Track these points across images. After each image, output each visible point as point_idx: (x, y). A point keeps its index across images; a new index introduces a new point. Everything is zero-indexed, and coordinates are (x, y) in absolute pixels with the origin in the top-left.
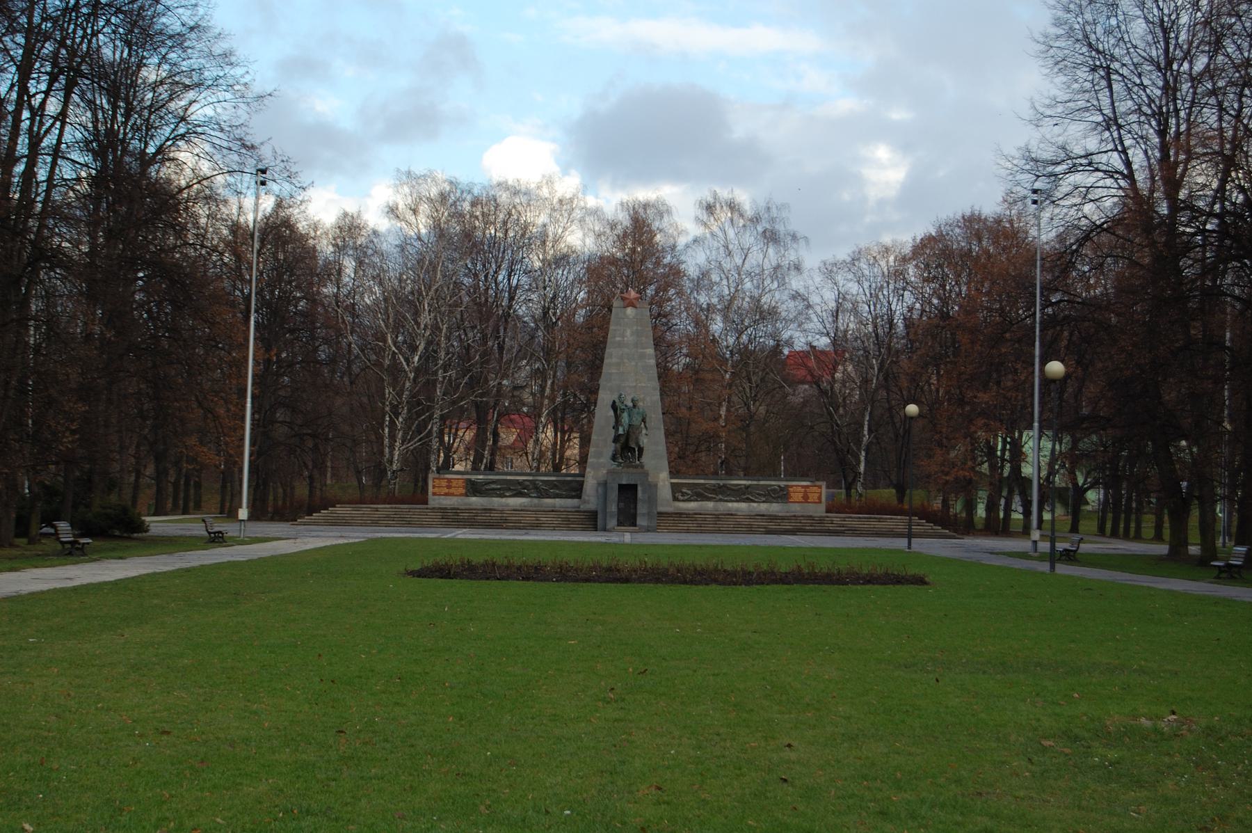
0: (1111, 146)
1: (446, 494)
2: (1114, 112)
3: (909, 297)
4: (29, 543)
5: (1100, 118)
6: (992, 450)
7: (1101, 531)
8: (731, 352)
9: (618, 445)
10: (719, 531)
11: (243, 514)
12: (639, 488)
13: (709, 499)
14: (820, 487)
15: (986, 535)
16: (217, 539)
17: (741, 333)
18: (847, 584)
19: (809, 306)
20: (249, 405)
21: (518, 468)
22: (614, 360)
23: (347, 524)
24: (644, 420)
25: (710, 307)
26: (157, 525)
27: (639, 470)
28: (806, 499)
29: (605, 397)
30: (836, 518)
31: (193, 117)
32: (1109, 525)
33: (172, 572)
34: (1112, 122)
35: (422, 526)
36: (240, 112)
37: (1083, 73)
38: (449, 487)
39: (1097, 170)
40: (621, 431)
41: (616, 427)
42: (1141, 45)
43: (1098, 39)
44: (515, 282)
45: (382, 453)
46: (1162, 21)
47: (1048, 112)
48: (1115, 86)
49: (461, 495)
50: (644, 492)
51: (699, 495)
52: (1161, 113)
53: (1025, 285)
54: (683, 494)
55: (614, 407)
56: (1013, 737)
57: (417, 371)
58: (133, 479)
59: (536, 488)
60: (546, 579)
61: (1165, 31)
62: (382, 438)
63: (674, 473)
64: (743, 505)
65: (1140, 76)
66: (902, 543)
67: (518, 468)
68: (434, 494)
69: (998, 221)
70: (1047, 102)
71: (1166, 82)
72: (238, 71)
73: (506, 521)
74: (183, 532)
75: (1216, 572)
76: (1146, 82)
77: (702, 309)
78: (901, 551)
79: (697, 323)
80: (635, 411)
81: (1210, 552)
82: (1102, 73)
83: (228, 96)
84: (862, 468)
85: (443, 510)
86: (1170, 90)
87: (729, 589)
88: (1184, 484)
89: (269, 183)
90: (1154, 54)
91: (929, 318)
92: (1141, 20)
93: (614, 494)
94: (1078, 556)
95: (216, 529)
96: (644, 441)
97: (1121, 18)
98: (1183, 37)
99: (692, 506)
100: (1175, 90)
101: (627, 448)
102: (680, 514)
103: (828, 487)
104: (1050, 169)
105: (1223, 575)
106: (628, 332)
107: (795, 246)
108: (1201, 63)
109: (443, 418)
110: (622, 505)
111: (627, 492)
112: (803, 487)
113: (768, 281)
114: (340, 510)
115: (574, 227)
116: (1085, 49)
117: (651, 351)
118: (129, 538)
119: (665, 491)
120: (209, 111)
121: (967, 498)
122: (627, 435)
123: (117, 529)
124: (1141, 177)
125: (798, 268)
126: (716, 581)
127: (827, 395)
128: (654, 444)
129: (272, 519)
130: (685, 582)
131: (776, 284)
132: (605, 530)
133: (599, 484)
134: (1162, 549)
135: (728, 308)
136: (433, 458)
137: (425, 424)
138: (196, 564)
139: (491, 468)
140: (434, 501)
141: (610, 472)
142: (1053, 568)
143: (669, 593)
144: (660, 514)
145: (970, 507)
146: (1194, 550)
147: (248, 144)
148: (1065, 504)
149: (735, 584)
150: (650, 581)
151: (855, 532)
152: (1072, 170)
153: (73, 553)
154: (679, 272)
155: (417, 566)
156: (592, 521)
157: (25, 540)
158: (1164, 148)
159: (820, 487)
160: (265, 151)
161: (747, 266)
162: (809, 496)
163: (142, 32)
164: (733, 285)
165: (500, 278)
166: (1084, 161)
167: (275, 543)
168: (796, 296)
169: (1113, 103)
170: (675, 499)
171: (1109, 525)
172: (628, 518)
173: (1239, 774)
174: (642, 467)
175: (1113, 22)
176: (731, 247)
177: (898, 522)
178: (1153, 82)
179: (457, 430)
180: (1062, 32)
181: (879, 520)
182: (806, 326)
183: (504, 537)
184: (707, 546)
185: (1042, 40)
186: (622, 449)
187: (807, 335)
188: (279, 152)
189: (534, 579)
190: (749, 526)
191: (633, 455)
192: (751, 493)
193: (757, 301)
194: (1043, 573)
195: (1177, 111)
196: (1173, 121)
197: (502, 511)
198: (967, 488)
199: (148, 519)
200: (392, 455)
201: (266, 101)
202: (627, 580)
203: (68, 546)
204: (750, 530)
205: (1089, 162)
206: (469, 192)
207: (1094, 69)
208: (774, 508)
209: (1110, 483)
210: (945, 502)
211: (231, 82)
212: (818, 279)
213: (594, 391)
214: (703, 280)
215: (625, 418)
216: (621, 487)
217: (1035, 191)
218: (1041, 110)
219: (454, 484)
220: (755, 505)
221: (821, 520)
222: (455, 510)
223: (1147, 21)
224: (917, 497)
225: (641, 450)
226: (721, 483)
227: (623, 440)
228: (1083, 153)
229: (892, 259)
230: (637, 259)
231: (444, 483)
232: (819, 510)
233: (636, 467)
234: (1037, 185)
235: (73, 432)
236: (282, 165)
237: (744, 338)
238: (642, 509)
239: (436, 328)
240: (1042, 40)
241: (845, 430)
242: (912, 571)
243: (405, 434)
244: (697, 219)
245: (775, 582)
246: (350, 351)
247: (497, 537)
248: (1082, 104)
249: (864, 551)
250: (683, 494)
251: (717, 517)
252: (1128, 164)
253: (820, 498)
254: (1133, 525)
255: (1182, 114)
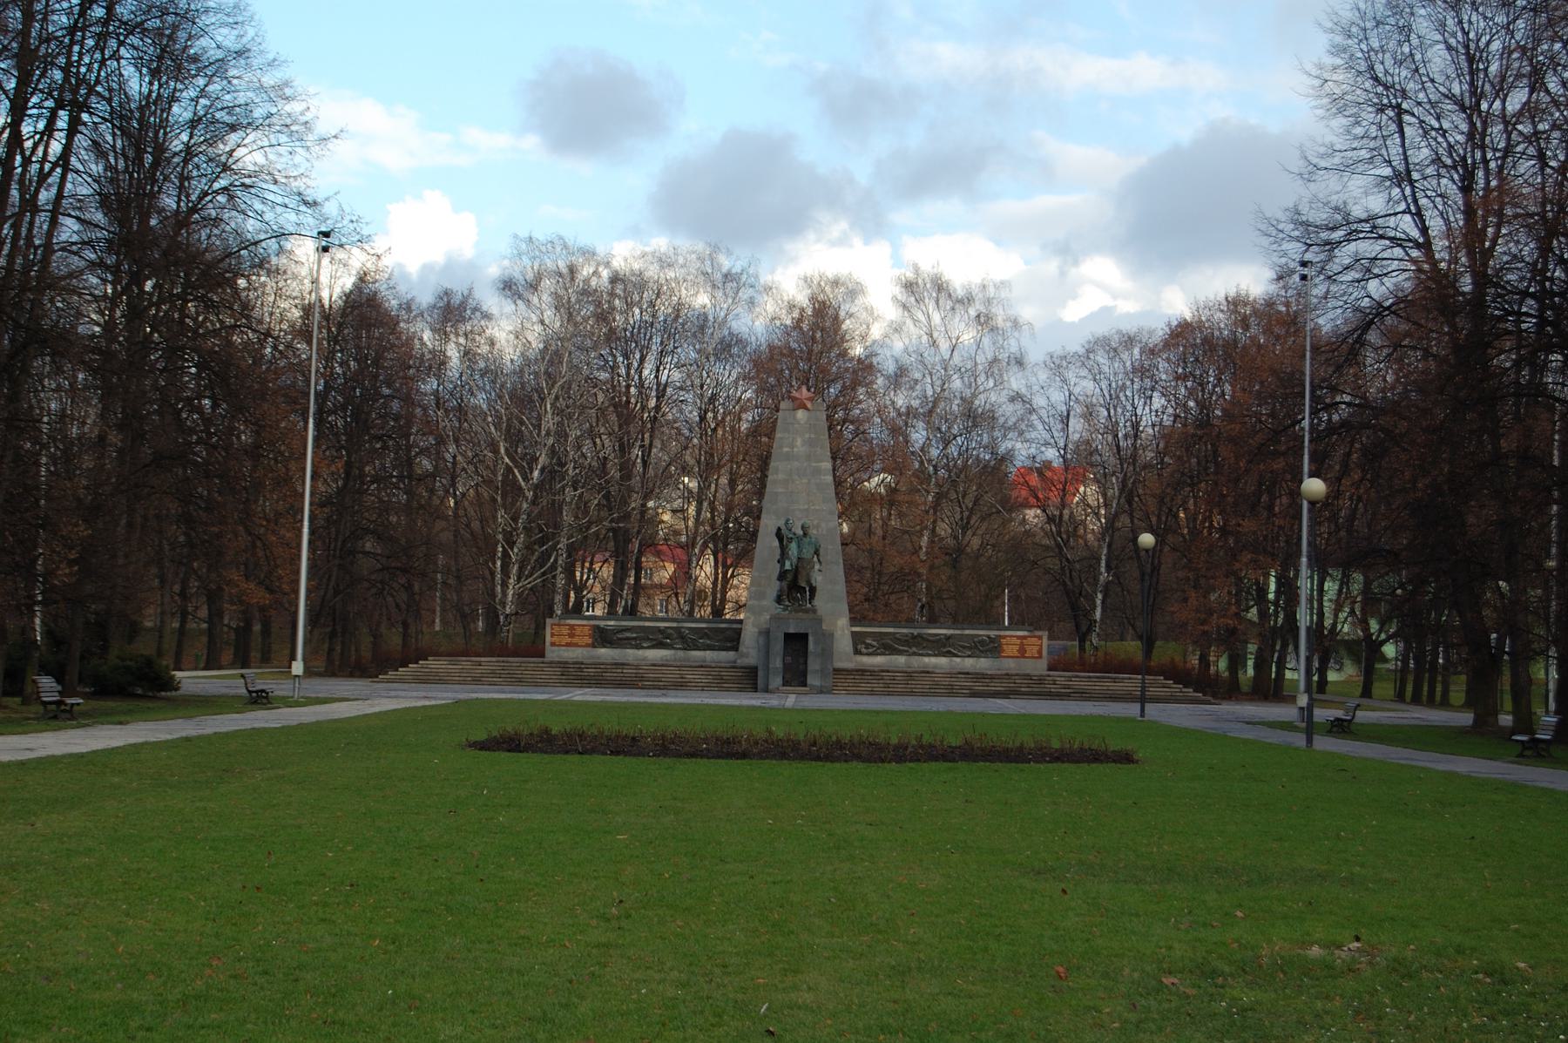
0: (1403, 206)
1: (568, 645)
2: (1407, 163)
3: (1158, 402)
4: (23, 703)
5: (1387, 171)
6: (1263, 591)
7: (1400, 697)
8: (935, 467)
9: (785, 584)
10: (912, 693)
11: (298, 667)
12: (811, 638)
13: (900, 653)
14: (1040, 638)
15: (1252, 700)
16: (259, 699)
17: (947, 443)
18: (1029, 761)
19: (1032, 411)
20: (306, 530)
21: (656, 611)
22: (781, 476)
23: (441, 681)
24: (817, 552)
25: (910, 412)
26: (190, 680)
27: (811, 616)
28: (1022, 652)
29: (769, 524)
30: (1060, 677)
31: (240, 165)
32: (1409, 688)
33: (172, 741)
34: (1403, 177)
35: (536, 685)
36: (297, 159)
37: (1369, 115)
38: (571, 635)
39: (1381, 237)
40: (788, 566)
41: (781, 561)
42: (1439, 79)
43: (1386, 72)
44: (664, 378)
45: (493, 596)
46: (1467, 47)
47: (1323, 164)
48: (1408, 130)
49: (587, 645)
50: (816, 643)
51: (887, 646)
52: (1465, 165)
53: (1292, 383)
54: (868, 646)
55: (779, 534)
56: (1127, 971)
57: (537, 488)
58: (176, 625)
59: (682, 637)
60: (641, 753)
61: (1471, 60)
62: (493, 574)
63: (854, 621)
64: (943, 661)
65: (1438, 119)
66: (1133, 709)
67: (656, 611)
68: (553, 644)
69: (1270, 303)
70: (1322, 150)
71: (1472, 125)
72: (294, 107)
73: (642, 679)
74: (224, 691)
75: (1519, 748)
76: (1446, 125)
77: (900, 415)
78: (1133, 720)
79: (895, 431)
80: (806, 540)
81: (1525, 721)
82: (1392, 114)
83: (283, 138)
84: (1098, 614)
85: (563, 664)
86: (1476, 137)
87: (873, 768)
88: (1494, 636)
89: (333, 250)
90: (1456, 89)
91: (1185, 425)
92: (1442, 46)
93: (778, 646)
94: (1353, 727)
95: (259, 687)
96: (818, 579)
97: (1415, 41)
98: (1494, 68)
99: (879, 660)
100: (1483, 135)
101: (795, 587)
102: (862, 672)
103: (1050, 638)
104: (1324, 235)
105: (1528, 753)
106: (799, 442)
107: (1016, 334)
108: (1517, 99)
109: (571, 549)
110: (789, 659)
111: (796, 643)
112: (1018, 637)
113: (982, 378)
114: (434, 664)
115: (740, 309)
116: (1368, 84)
117: (828, 465)
118: (154, 697)
119: (843, 643)
120: (259, 158)
121: (1228, 655)
122: (796, 571)
123: (141, 685)
124: (1439, 245)
125: (1020, 363)
126: (858, 757)
127: (1063, 527)
128: (830, 583)
129: (351, 675)
130: (818, 758)
131: (991, 383)
132: (766, 690)
133: (760, 633)
134: (1466, 718)
135: (931, 412)
136: (558, 598)
137: (545, 557)
138: (209, 731)
139: (632, 612)
140: (552, 654)
141: (774, 618)
142: (1310, 741)
143: (789, 770)
144: (837, 671)
145: (1236, 663)
146: (1506, 720)
147: (309, 199)
148: (1357, 661)
149: (883, 761)
150: (774, 757)
151: (1084, 696)
152: (1348, 239)
153: (58, 716)
154: (871, 366)
155: (481, 736)
156: (750, 679)
157: (18, 700)
158: (1469, 212)
159: (1040, 638)
160: (330, 209)
161: (957, 359)
162: (1026, 650)
163: (171, 59)
164: (939, 383)
165: (646, 372)
166: (1367, 227)
167: (335, 705)
168: (1016, 398)
169: (1405, 153)
170: (857, 652)
171: (1409, 688)
172: (796, 676)
173: (1408, 1027)
174: (815, 611)
175: (1406, 49)
176: (935, 335)
177: (1131, 683)
178: (1456, 124)
179: (591, 563)
180: (1339, 61)
181: (1114, 680)
182: (1028, 436)
183: (723, 702)
184: (887, 712)
185: (1315, 72)
186: (790, 588)
187: (1032, 447)
188: (347, 210)
189: (626, 754)
190: (950, 686)
191: (803, 597)
192: (952, 646)
193: (967, 402)
194: (1297, 749)
195: (1485, 162)
196: (1480, 174)
197: (637, 667)
198: (1232, 641)
199: (178, 674)
200: (505, 594)
201: (330, 146)
202: (744, 755)
203: (54, 707)
204: (951, 692)
205: (1372, 226)
206: (607, 264)
207: (1381, 110)
208: (982, 664)
209: (1413, 632)
210: (1204, 659)
211: (288, 121)
212: (1043, 376)
213: (756, 514)
214: (899, 377)
215: (793, 548)
216: (788, 636)
217: (1304, 264)
218: (1315, 161)
219: (578, 632)
220: (958, 660)
221: (1041, 680)
222: (579, 665)
223: (1449, 48)
224: (1166, 651)
225: (813, 590)
226: (916, 632)
227: (790, 577)
228: (1364, 216)
229: (1136, 351)
230: (814, 351)
231: (565, 631)
232: (1039, 667)
233: (807, 611)
234: (1308, 257)
235: (71, 563)
236: (351, 226)
237: (953, 450)
238: (813, 664)
239: (562, 435)
240: (1315, 72)
241: (1077, 566)
242: (1115, 745)
243: (521, 569)
244: (895, 299)
245: (935, 758)
246: (454, 463)
247: (625, 699)
248: (1364, 154)
249: (1050, 720)
250: (868, 646)
251: (909, 675)
252: (1424, 230)
253: (1040, 652)
254: (1439, 688)
255: (1493, 165)
